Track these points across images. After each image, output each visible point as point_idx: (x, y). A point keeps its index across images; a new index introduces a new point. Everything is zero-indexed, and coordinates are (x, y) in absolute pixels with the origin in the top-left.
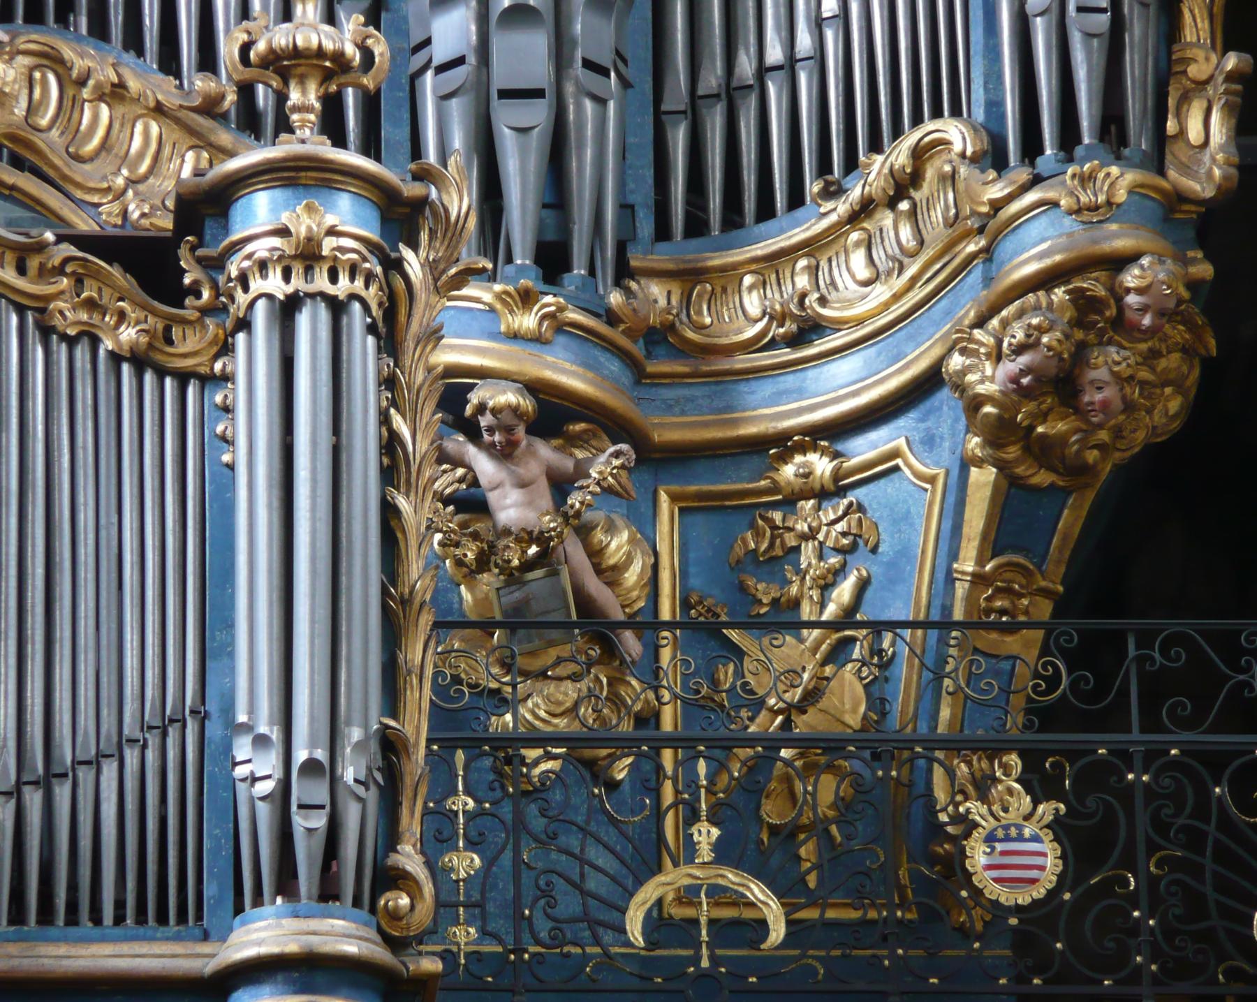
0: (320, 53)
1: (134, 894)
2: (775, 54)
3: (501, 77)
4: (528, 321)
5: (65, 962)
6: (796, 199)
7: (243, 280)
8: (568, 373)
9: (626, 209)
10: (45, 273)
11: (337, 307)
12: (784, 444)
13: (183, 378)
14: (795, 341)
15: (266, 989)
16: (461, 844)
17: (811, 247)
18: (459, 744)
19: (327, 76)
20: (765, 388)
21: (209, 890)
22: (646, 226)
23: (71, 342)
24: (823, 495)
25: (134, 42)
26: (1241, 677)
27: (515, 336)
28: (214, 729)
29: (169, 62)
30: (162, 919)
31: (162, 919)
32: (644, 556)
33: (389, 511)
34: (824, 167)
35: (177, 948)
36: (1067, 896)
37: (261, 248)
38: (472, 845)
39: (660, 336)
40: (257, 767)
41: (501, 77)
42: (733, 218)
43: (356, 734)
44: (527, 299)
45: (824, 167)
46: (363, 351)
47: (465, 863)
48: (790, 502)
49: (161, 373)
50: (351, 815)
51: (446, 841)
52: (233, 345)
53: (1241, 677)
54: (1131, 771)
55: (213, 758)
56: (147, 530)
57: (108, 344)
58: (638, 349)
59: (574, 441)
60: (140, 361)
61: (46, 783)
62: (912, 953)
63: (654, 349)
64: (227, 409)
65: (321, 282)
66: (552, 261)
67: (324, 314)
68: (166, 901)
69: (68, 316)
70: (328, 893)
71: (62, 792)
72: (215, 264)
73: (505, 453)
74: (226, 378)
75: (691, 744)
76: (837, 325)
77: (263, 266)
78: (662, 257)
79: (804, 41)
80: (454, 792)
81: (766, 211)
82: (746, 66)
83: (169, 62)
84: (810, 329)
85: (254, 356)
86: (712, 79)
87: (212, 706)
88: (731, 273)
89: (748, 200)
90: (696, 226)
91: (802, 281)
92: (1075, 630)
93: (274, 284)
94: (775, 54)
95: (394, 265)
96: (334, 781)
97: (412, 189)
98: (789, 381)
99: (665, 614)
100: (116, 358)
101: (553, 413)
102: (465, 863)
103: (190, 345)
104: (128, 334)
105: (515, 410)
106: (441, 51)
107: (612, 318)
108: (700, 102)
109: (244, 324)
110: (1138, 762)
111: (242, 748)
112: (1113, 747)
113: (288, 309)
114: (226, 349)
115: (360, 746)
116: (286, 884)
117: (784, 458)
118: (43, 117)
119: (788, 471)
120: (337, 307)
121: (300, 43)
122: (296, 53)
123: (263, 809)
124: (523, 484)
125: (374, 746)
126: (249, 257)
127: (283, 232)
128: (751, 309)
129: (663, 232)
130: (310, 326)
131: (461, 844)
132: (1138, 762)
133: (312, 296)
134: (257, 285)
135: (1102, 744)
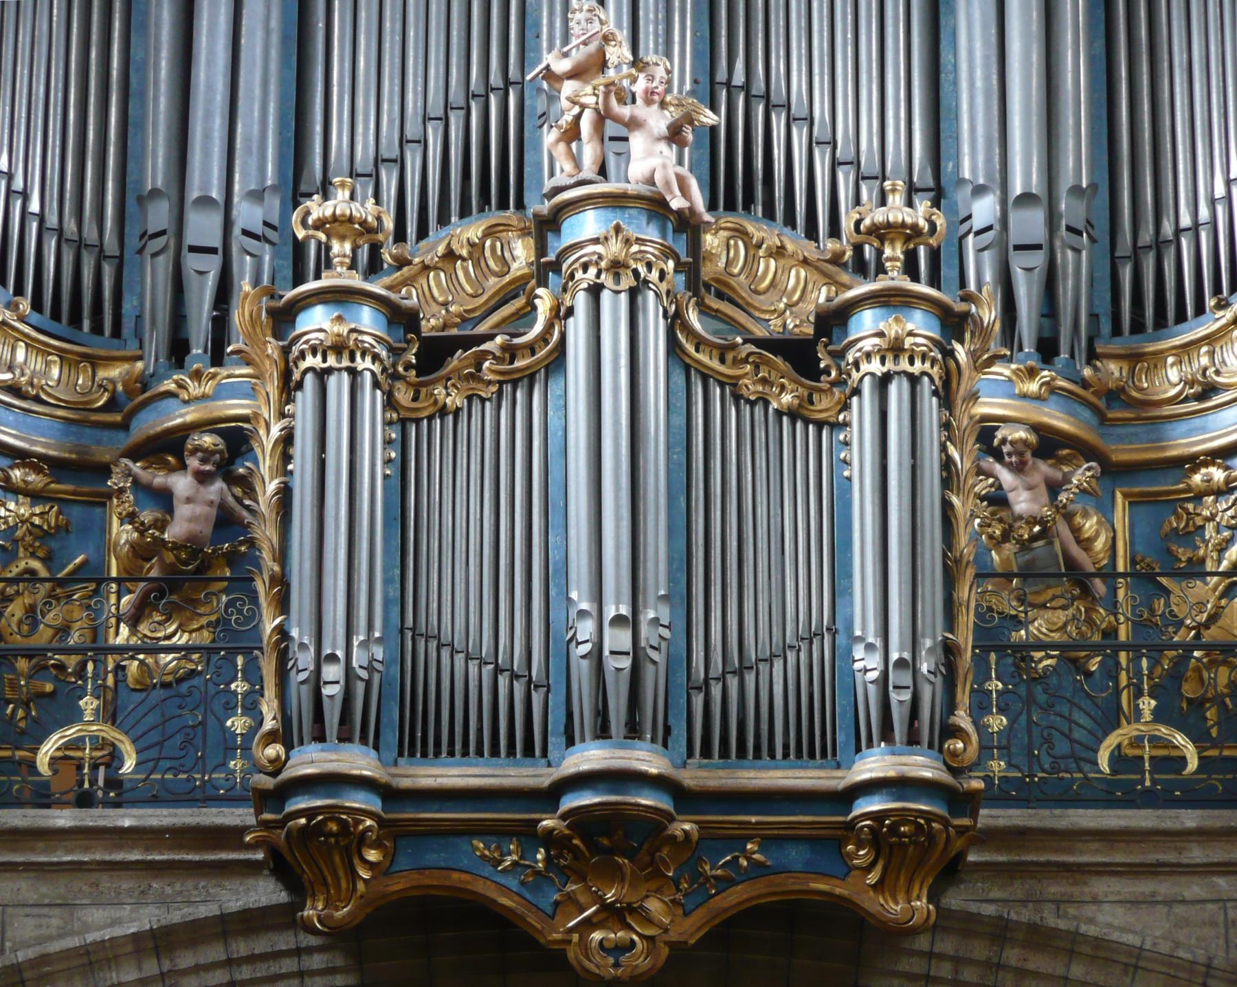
2: (1186, 221)
3: (1014, 239)
4: (1033, 387)
6: (1200, 310)
7: (856, 364)
8: (1058, 419)
9: (1094, 317)
10: (737, 362)
11: (914, 380)
12: (1194, 462)
13: (820, 425)
14: (1201, 397)
17: (1210, 339)
19: (908, 239)
20: (1182, 427)
21: (840, 738)
22: (1106, 327)
23: (753, 404)
24: (1220, 492)
25: (790, 221)
27: (1024, 396)
28: (841, 640)
29: (811, 232)
30: (465, 753)
32: (1108, 532)
33: (947, 506)
34: (1217, 290)
37: (867, 345)
38: (1001, 711)
39: (1116, 395)
40: (867, 663)
42: (1161, 321)
43: (928, 643)
44: (1032, 373)
45: (1217, 290)
46: (930, 406)
48: (1198, 497)
49: (807, 422)
50: (926, 693)
55: (842, 656)
56: (798, 519)
57: (774, 405)
58: (1101, 404)
59: (1062, 461)
60: (794, 415)
61: (740, 673)
63: (1113, 404)
64: (846, 444)
65: (904, 365)
66: (1047, 349)
67: (906, 384)
68: (814, 745)
69: (751, 388)
71: (750, 678)
72: (839, 355)
73: (1019, 469)
74: (846, 424)
76: (1227, 387)
77: (868, 356)
78: (1116, 346)
79: (1204, 213)
81: (1181, 317)
82: (1168, 229)
83: (811, 232)
84: (1210, 390)
85: (863, 412)
86: (1146, 236)
87: (840, 625)
88: (1160, 356)
89: (1170, 312)
90: (1138, 327)
91: (1205, 361)
93: (875, 367)
94: (1186, 221)
95: (949, 354)
96: (915, 672)
97: (960, 307)
98: (1197, 422)
99: (1121, 568)
100: (779, 414)
101: (1048, 444)
103: (824, 405)
104: (787, 399)
105: (1024, 442)
106: (978, 222)
107: (1085, 384)
109: (857, 391)
111: (859, 652)
113: (322, 375)
114: (846, 407)
115: (931, 651)
116: (887, 734)
117: (1195, 470)
119: (1197, 478)
120: (914, 380)
122: (889, 225)
123: (872, 689)
124: (1030, 488)
125: (939, 651)
127: (881, 334)
128: (1172, 378)
129: (1117, 331)
130: (897, 392)
134: (865, 367)
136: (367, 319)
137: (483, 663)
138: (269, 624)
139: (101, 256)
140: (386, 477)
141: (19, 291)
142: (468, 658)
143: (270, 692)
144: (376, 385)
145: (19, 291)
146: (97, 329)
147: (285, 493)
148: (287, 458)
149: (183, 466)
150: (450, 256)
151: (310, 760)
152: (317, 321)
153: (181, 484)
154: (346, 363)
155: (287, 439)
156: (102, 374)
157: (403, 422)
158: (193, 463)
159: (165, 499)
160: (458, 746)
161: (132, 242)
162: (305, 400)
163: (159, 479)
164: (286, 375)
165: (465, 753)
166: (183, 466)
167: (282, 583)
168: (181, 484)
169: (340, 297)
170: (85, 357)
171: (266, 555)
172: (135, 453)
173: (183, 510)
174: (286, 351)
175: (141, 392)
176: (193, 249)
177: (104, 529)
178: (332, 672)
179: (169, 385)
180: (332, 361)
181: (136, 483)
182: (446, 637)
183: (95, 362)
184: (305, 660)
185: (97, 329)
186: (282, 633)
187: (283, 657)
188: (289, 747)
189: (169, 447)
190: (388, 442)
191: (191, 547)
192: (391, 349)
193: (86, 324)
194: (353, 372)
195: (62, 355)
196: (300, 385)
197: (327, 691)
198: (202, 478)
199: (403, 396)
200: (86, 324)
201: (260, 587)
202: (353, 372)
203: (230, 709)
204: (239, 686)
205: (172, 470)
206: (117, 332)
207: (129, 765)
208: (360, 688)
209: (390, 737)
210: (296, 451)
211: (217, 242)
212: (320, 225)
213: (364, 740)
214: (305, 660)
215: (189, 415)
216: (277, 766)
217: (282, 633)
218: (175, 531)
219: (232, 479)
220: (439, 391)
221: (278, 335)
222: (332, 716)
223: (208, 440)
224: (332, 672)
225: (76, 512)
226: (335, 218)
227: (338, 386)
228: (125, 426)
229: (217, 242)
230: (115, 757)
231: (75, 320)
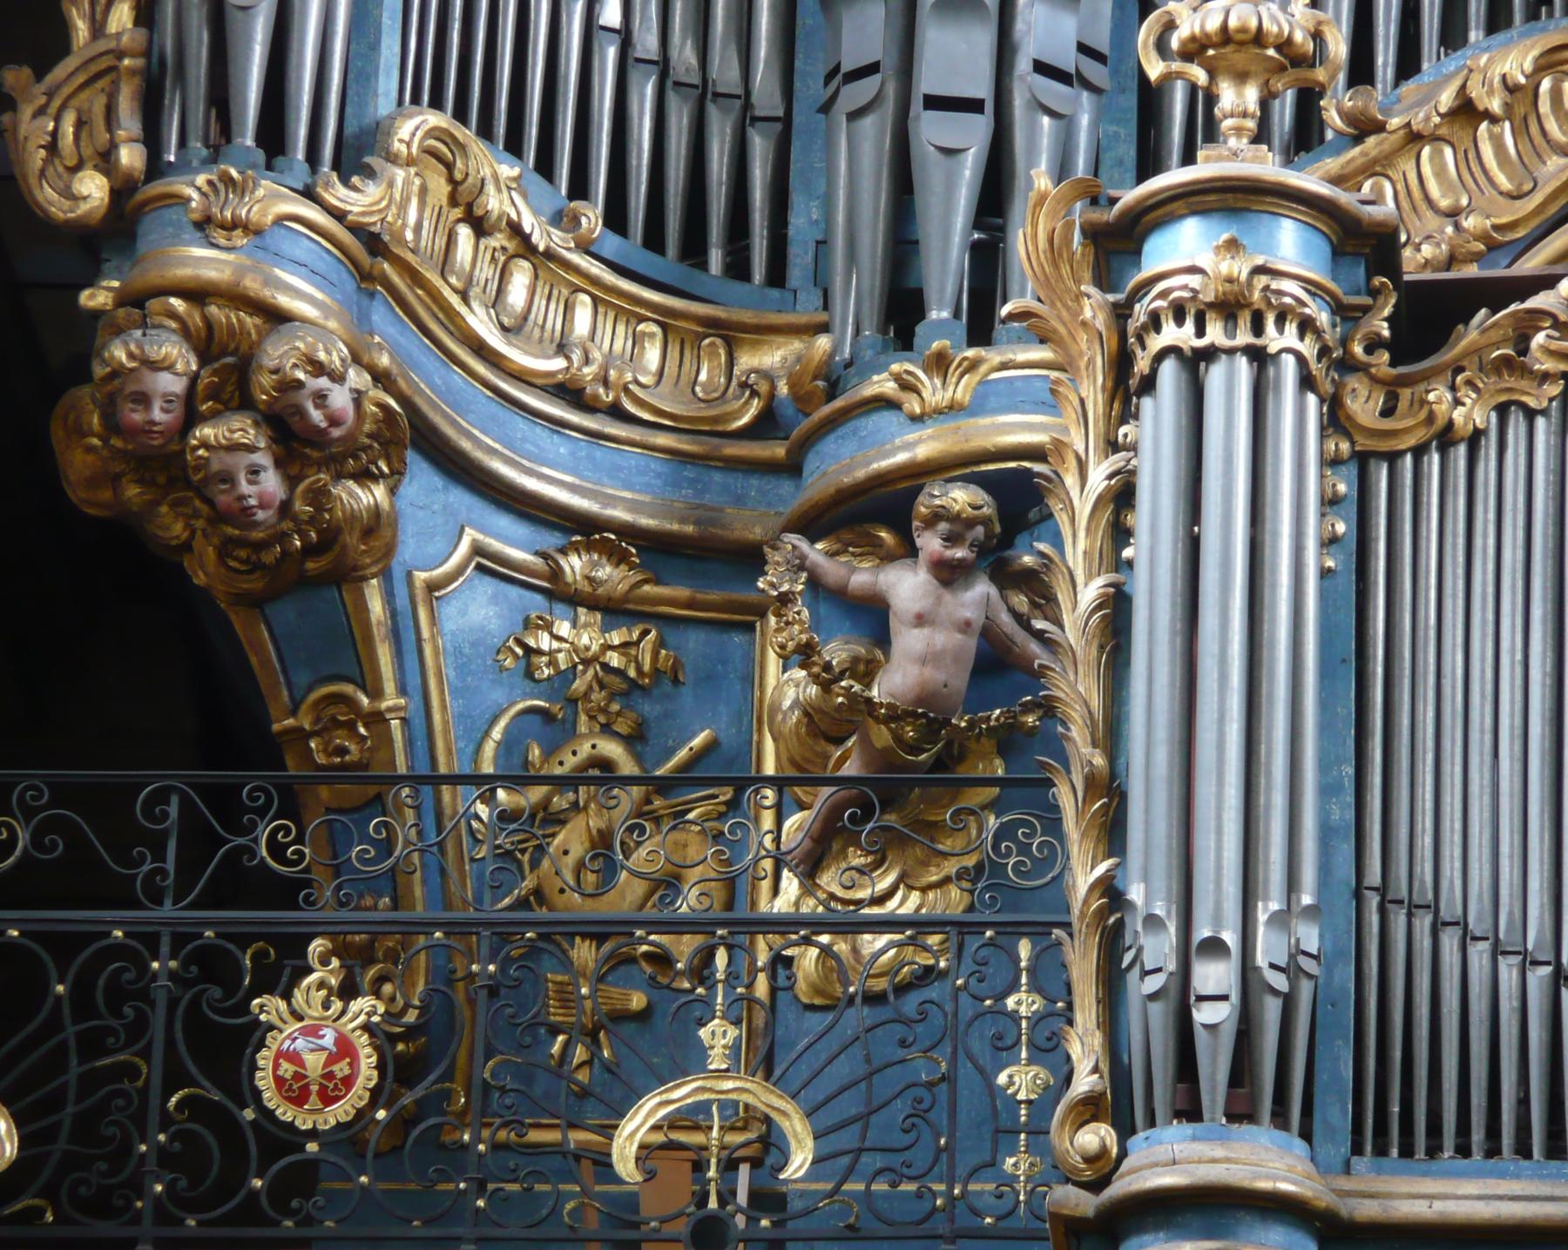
0: (1259, 38)
1: (1513, 1116)
3: (929, 81)
5: (1439, 1206)
15: (1147, 1238)
16: (1024, 1054)
18: (321, 929)
26: (240, 841)
30: (1493, 1151)
31: (1464, 1150)
35: (1516, 1187)
36: (381, 1114)
41: (929, 81)
47: (1021, 1079)
51: (1007, 1049)
52: (1137, 408)
53: (240, 841)
54: (156, 958)
62: (451, 1186)
70: (1240, 1113)
75: (709, 929)
80: (1014, 987)
92: (46, 783)
102: (1021, 1079)
108: (780, 113)
110: (165, 948)
112: (221, 930)
113: (1196, 362)
118: (243, 136)
121: (1233, 23)
126: (1163, 295)
131: (1024, 1054)
132: (165, 948)
133: (1231, 352)
135: (118, 924)
136: (1290, 245)
137: (1528, 962)
138: (1084, 875)
139: (747, 118)
140: (1325, 573)
141: (580, 188)
142: (1497, 951)
143: (1087, 1014)
144: (1307, 382)
145: (580, 188)
146: (738, 268)
147: (1117, 606)
148: (1121, 534)
149: (910, 550)
150: (1466, 112)
151: (1168, 1157)
152: (1185, 251)
153: (906, 586)
154: (1244, 337)
155: (1123, 495)
156: (747, 360)
157: (1363, 460)
158: (930, 543)
159: (872, 616)
160: (1478, 1136)
161: (810, 88)
162: (1159, 416)
163: (862, 576)
164: (1121, 362)
165: (1493, 1151)
166: (910, 550)
167: (1109, 791)
168: (906, 586)
169: (1234, 199)
170: (713, 325)
171: (1078, 733)
172: (812, 524)
173: (908, 641)
174: (1120, 313)
175: (827, 397)
176: (935, 103)
177: (751, 677)
178: (1213, 976)
179: (882, 384)
180: (1215, 333)
181: (815, 584)
182: (1450, 907)
183: (731, 335)
184: (1159, 949)
185: (738, 268)
186: (1111, 893)
187: (1112, 943)
188: (1126, 1130)
189: (879, 512)
190: (1330, 502)
191: (926, 714)
192: (1339, 309)
193: (716, 258)
194: (1259, 356)
195: (667, 322)
196: (1149, 384)
197: (1204, 1015)
198: (949, 574)
199: (1363, 405)
200: (716, 258)
201: (1066, 798)
202: (1259, 356)
203: (1004, 1049)
204: (1023, 1003)
205: (888, 558)
206: (777, 275)
207: (800, 1161)
208: (1272, 1010)
209: (1335, 1113)
210: (1140, 519)
211: (982, 89)
212: (1194, 50)
213: (1280, 1118)
214: (1159, 949)
215: (923, 445)
216: (1102, 1169)
217: (1111, 893)
218: (894, 683)
219: (1008, 577)
220: (1438, 395)
221: (1104, 281)
222: (1214, 1068)
223: (960, 497)
224: (1213, 976)
225: (694, 642)
226: (1225, 36)
227: (1229, 385)
228: (792, 468)
229: (982, 89)
230: (770, 1146)
231: (694, 251)
